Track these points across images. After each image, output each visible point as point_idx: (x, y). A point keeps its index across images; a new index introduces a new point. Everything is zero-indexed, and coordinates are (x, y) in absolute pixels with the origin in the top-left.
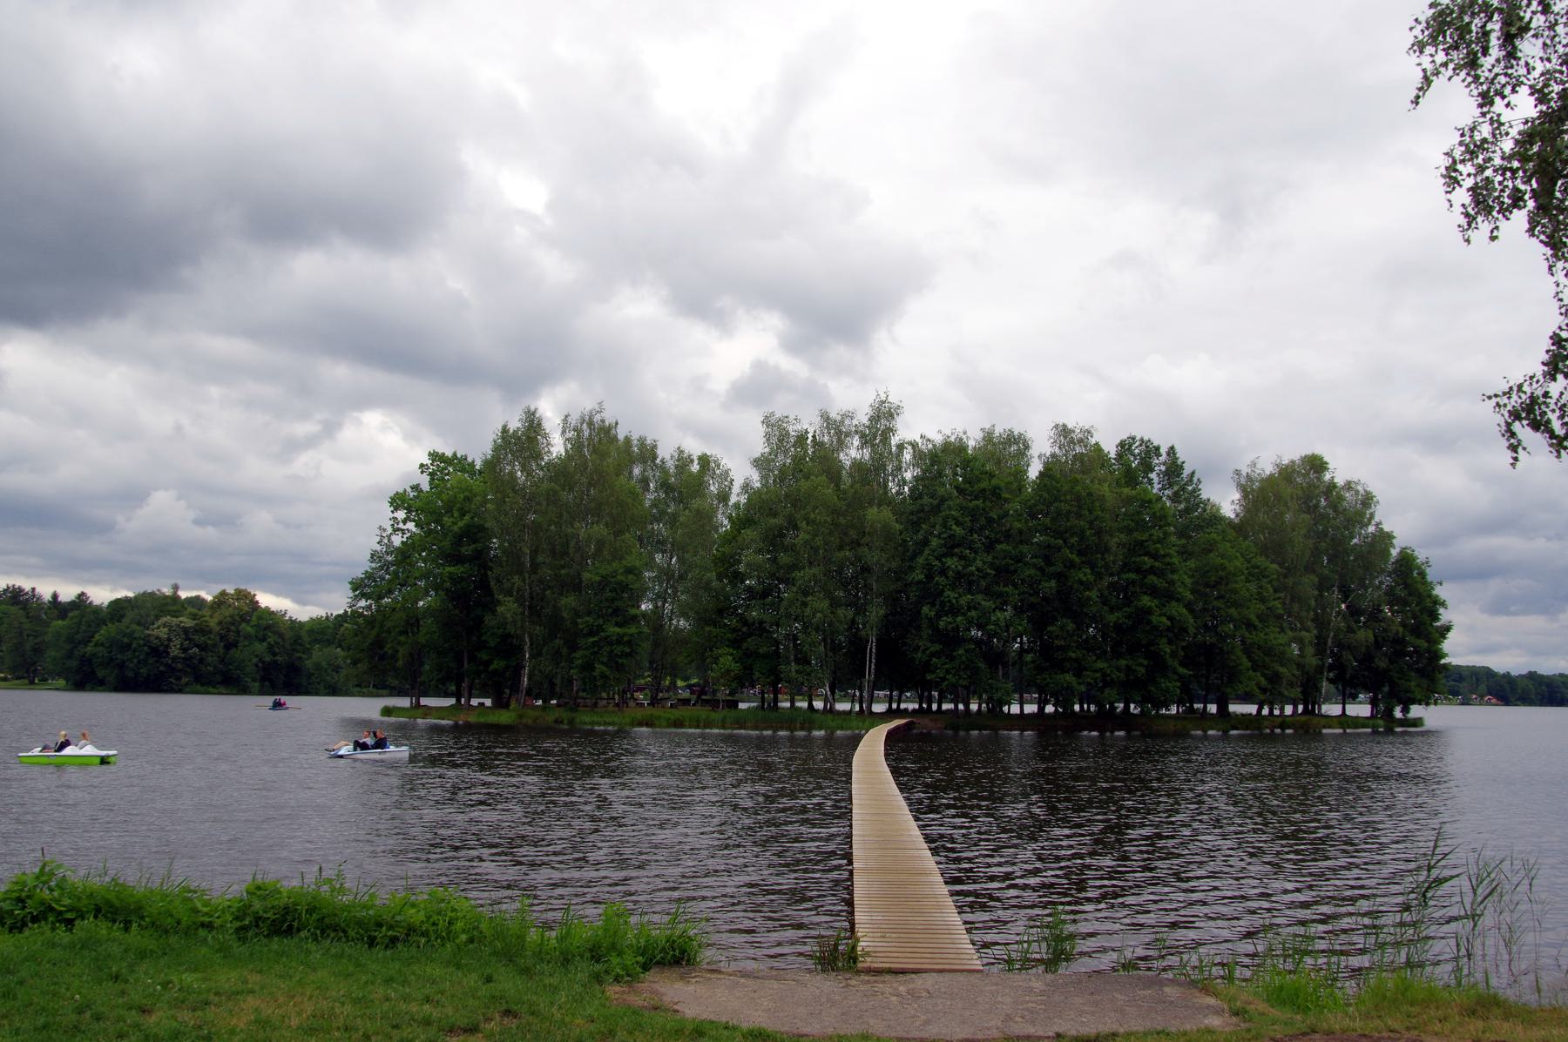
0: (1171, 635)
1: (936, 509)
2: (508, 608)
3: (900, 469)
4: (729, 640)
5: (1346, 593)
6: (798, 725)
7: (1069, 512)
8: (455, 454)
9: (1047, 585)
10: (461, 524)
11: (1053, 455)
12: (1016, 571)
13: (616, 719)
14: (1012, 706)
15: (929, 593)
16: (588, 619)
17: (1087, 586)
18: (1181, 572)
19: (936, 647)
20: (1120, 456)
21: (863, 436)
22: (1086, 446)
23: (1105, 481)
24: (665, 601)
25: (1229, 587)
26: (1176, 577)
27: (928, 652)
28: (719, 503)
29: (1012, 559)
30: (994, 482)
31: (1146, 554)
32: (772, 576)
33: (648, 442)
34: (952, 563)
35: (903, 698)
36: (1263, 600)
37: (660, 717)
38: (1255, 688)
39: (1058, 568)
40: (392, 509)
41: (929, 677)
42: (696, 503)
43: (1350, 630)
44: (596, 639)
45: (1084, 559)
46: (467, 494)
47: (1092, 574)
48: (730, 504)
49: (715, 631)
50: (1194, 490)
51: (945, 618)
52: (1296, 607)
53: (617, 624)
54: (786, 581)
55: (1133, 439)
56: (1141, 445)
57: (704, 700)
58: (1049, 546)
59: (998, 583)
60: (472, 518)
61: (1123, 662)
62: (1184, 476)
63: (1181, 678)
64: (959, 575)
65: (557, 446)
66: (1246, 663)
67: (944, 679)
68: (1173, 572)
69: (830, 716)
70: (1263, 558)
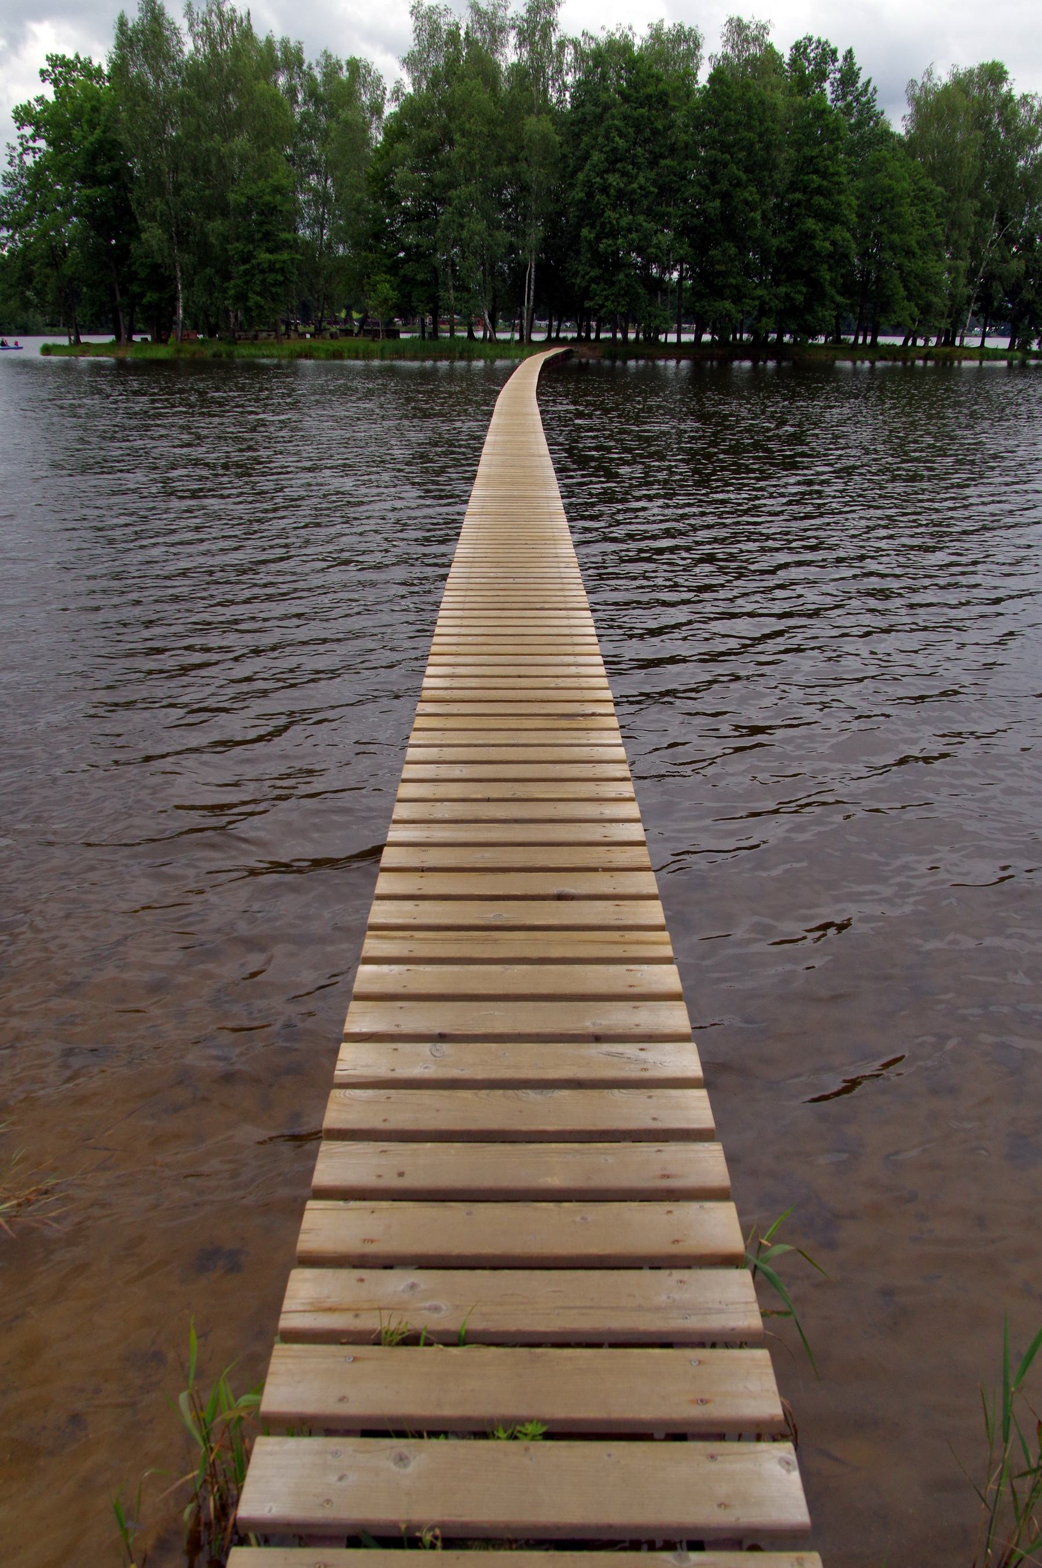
0: (832, 261)
1: (599, 119)
2: (153, 235)
3: (561, 71)
4: (385, 266)
5: (1003, 221)
6: (457, 355)
7: (739, 123)
8: (77, 57)
9: (711, 204)
10: (91, 139)
11: (725, 57)
12: (679, 190)
13: (275, 352)
14: (669, 336)
15: (589, 214)
16: (237, 245)
17: (752, 206)
18: (848, 192)
19: (595, 272)
20: (794, 61)
21: (520, 33)
22: (760, 46)
23: (777, 87)
24: (322, 228)
25: (893, 211)
26: (842, 198)
27: (587, 277)
28: (372, 115)
29: (675, 175)
30: (660, 87)
31: (816, 172)
32: (427, 195)
33: (292, 44)
34: (613, 179)
35: (563, 327)
36: (925, 225)
37: (318, 348)
38: (908, 318)
39: (724, 186)
40: (18, 124)
41: (587, 304)
42: (344, 114)
43: (1004, 260)
44: (247, 266)
45: (751, 176)
46: (94, 103)
47: (758, 193)
48: (384, 117)
49: (371, 256)
50: (868, 102)
51: (604, 241)
52: (955, 234)
53: (269, 251)
54: (441, 201)
55: (810, 39)
56: (817, 48)
57: (365, 331)
58: (715, 162)
59: (660, 204)
60: (104, 132)
61: (782, 290)
62: (859, 85)
63: (838, 306)
64: (621, 194)
65: (189, 46)
66: (902, 292)
67: (602, 306)
68: (840, 192)
69: (488, 346)
70: (930, 180)
